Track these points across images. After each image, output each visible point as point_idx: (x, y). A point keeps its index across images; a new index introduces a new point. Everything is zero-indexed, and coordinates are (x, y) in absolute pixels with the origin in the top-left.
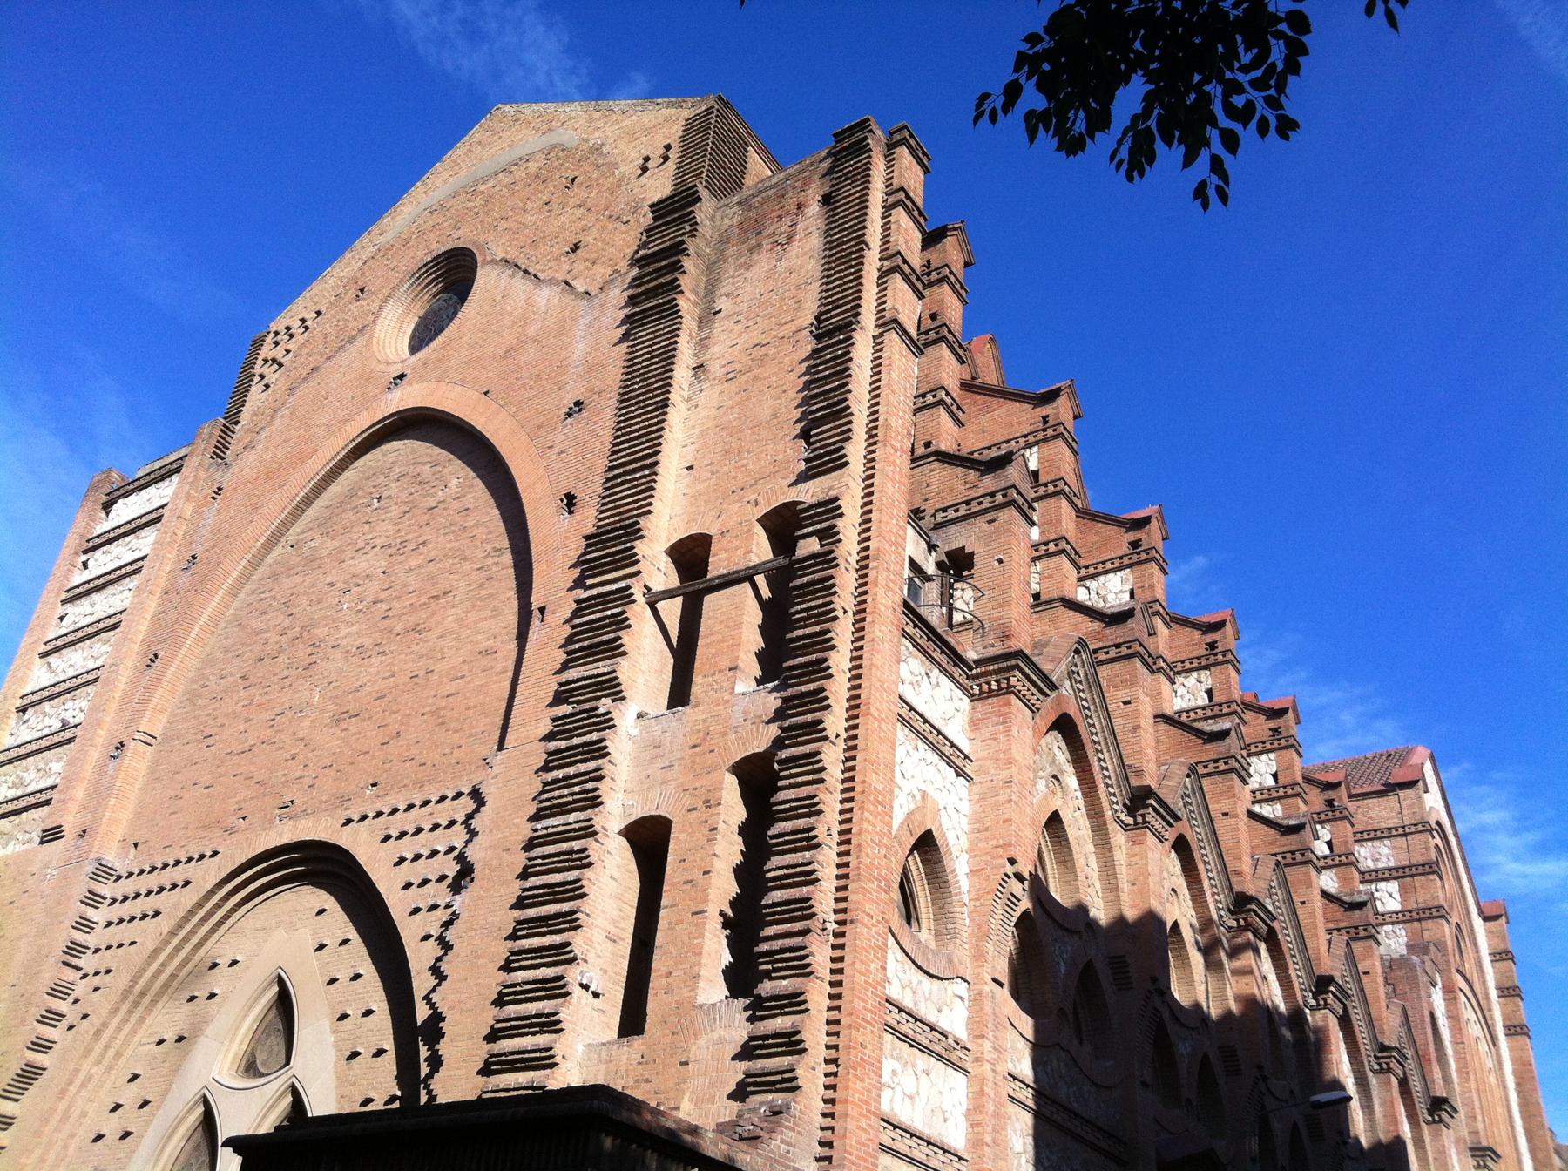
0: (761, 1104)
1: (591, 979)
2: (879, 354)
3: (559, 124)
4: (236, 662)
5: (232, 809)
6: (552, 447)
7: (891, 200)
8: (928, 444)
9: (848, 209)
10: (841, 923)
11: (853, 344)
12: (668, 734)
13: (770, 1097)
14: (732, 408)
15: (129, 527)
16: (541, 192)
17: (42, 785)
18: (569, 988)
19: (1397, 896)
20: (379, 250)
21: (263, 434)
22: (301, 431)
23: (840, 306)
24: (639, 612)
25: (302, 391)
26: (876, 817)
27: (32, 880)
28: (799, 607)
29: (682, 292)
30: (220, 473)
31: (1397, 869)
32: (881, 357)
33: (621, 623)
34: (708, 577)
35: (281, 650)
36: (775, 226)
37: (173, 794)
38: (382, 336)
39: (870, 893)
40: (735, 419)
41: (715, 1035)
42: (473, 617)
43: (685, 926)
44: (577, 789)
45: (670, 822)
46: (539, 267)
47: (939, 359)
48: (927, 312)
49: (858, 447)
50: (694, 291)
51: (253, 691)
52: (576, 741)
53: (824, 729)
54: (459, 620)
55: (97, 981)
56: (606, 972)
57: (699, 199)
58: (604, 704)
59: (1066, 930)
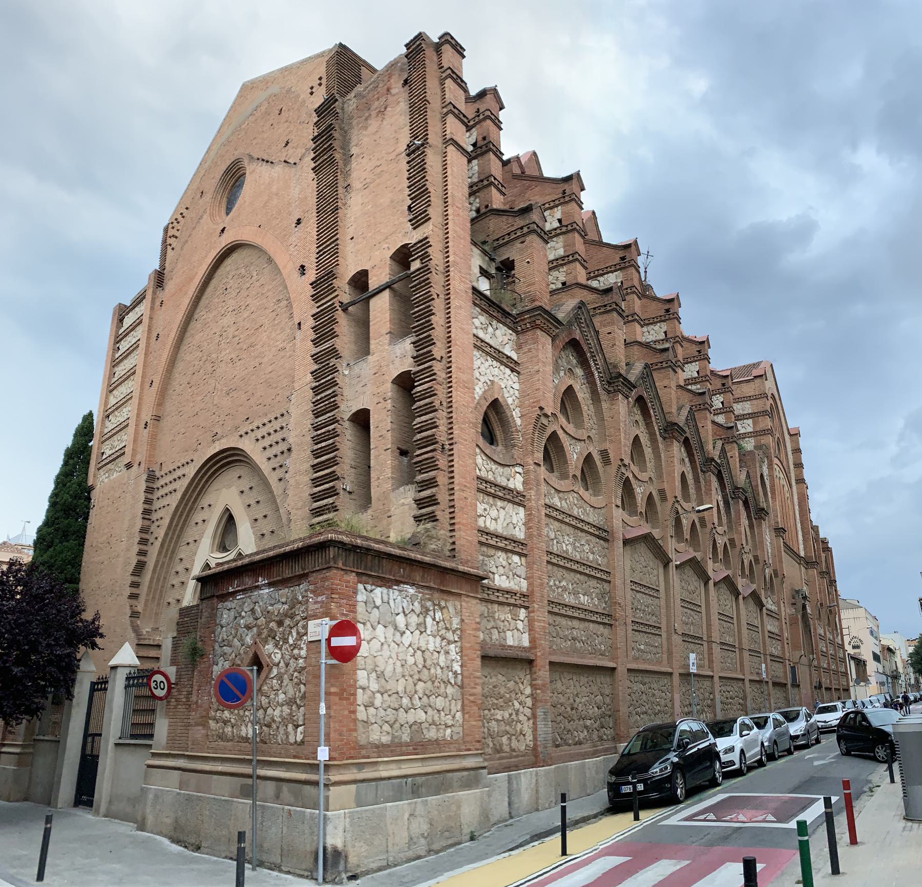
8: (487, 207)
15: (131, 327)
18: (337, 491)
19: (752, 426)
24: (340, 315)
31: (752, 414)
33: (334, 321)
34: (370, 290)
41: (401, 502)
44: (327, 402)
46: (273, 158)
47: (489, 160)
50: (342, 148)
52: (323, 381)
54: (268, 337)
57: (337, 100)
58: (333, 362)
59: (576, 439)
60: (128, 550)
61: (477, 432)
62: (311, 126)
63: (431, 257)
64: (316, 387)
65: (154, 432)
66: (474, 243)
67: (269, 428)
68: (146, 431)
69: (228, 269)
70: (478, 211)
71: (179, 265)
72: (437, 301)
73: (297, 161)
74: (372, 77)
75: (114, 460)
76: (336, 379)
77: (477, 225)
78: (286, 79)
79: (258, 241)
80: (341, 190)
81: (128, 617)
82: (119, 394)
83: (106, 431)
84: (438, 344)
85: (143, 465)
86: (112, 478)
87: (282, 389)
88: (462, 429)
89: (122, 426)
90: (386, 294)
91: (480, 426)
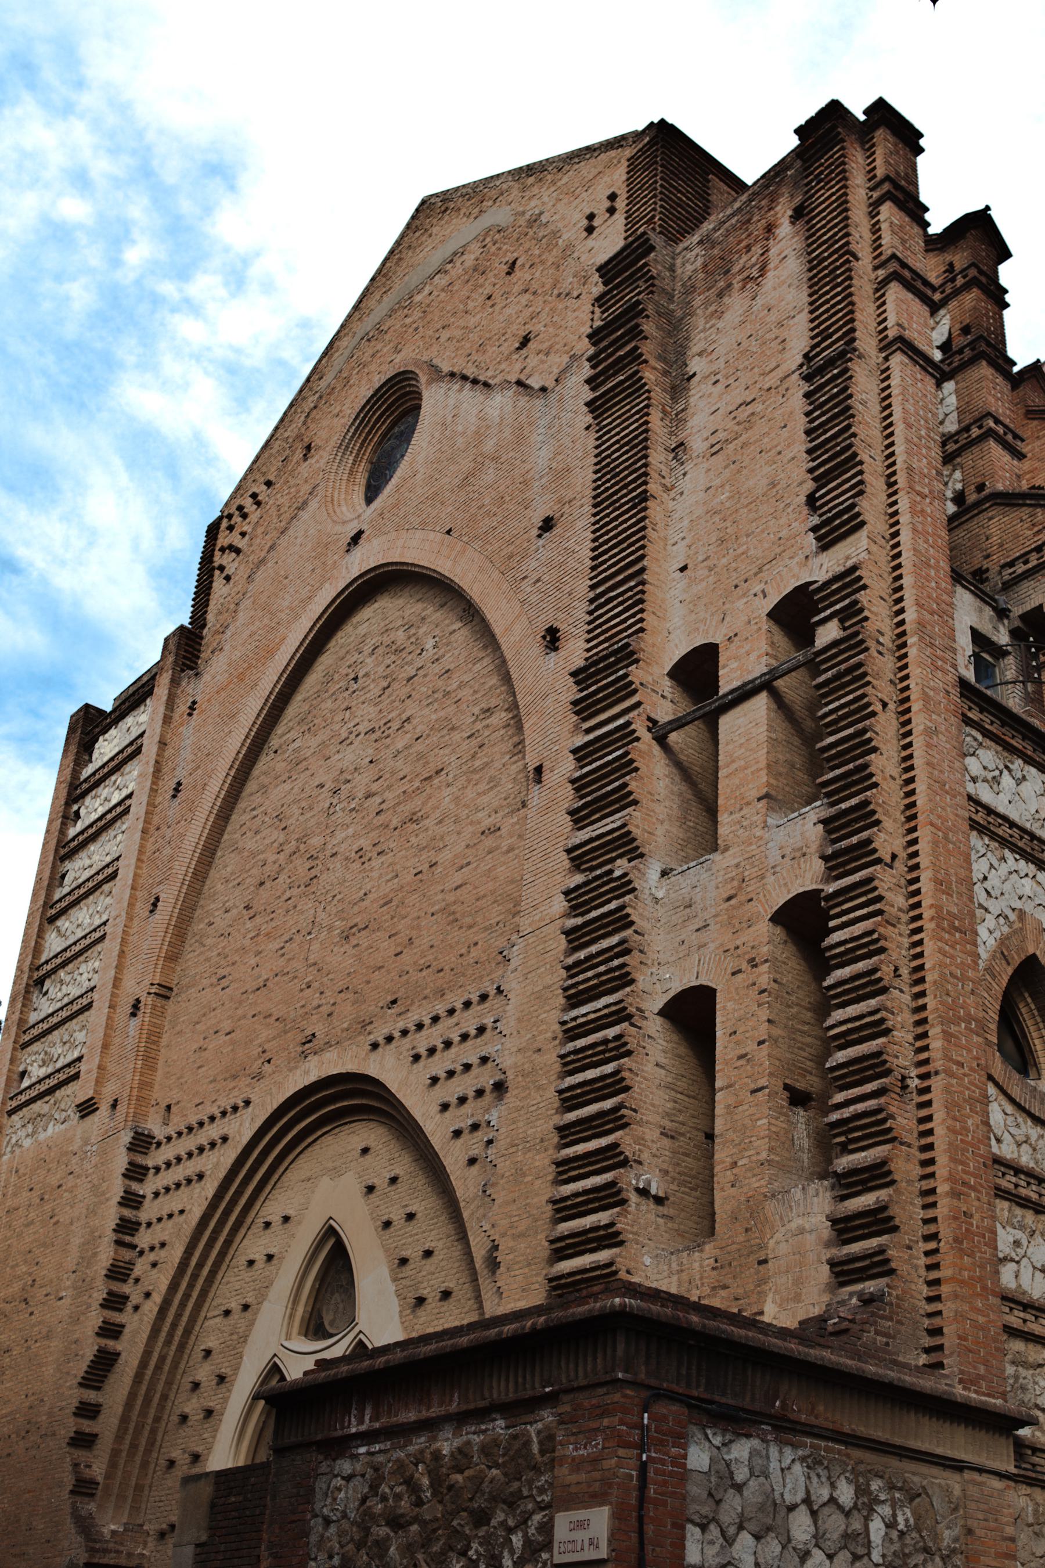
0: (851, 1295)
1: (648, 1182)
2: (886, 384)
3: (490, 203)
4: (237, 892)
5: (255, 1052)
6: (525, 577)
7: (876, 195)
8: (981, 488)
9: (824, 218)
10: (923, 1077)
11: (851, 377)
12: (698, 889)
13: (858, 1287)
14: (722, 486)
15: (112, 764)
16: (481, 286)
17: (69, 1058)
18: (623, 1195)
20: (321, 397)
21: (229, 633)
22: (266, 621)
23: (830, 336)
24: (646, 748)
25: (259, 576)
26: (953, 947)
27: (75, 1160)
28: (826, 709)
29: (646, 361)
30: (192, 685)
32: (889, 387)
33: (627, 766)
35: (281, 869)
36: (745, 258)
37: (195, 1046)
38: (336, 495)
39: (957, 1038)
40: (729, 498)
41: (793, 1225)
42: (470, 793)
43: (746, 1107)
44: (602, 969)
45: (714, 991)
46: (490, 373)
48: (958, 326)
49: (875, 501)
50: (661, 358)
51: (258, 920)
52: (594, 914)
53: (875, 851)
54: (457, 800)
55: (152, 1257)
56: (667, 1172)
57: (652, 248)
58: (621, 866)
60: (76, 1320)
61: (988, 1043)
62: (586, 305)
63: (866, 613)
64: (576, 929)
65: (155, 1025)
66: (957, 577)
67: (450, 1030)
68: (135, 1023)
69: (362, 630)
70: (959, 498)
71: (242, 617)
72: (882, 717)
73: (550, 383)
74: (735, 200)
75: (51, 1091)
76: (628, 910)
77: (960, 533)
78: (527, 194)
79: (444, 566)
80: (658, 457)
81: (65, 1494)
82: (72, 927)
83: (33, 1017)
84: (888, 824)
85: (121, 1108)
86: (42, 1136)
87: (486, 929)
88: (951, 1035)
89: (75, 1007)
90: (761, 704)
91: (994, 1026)
